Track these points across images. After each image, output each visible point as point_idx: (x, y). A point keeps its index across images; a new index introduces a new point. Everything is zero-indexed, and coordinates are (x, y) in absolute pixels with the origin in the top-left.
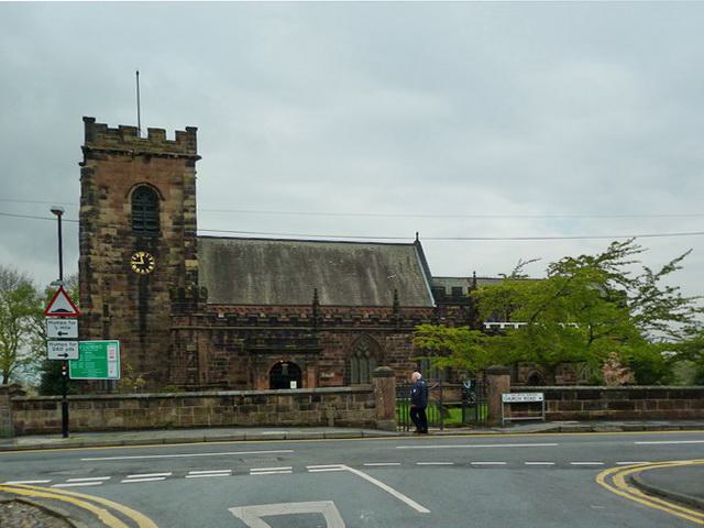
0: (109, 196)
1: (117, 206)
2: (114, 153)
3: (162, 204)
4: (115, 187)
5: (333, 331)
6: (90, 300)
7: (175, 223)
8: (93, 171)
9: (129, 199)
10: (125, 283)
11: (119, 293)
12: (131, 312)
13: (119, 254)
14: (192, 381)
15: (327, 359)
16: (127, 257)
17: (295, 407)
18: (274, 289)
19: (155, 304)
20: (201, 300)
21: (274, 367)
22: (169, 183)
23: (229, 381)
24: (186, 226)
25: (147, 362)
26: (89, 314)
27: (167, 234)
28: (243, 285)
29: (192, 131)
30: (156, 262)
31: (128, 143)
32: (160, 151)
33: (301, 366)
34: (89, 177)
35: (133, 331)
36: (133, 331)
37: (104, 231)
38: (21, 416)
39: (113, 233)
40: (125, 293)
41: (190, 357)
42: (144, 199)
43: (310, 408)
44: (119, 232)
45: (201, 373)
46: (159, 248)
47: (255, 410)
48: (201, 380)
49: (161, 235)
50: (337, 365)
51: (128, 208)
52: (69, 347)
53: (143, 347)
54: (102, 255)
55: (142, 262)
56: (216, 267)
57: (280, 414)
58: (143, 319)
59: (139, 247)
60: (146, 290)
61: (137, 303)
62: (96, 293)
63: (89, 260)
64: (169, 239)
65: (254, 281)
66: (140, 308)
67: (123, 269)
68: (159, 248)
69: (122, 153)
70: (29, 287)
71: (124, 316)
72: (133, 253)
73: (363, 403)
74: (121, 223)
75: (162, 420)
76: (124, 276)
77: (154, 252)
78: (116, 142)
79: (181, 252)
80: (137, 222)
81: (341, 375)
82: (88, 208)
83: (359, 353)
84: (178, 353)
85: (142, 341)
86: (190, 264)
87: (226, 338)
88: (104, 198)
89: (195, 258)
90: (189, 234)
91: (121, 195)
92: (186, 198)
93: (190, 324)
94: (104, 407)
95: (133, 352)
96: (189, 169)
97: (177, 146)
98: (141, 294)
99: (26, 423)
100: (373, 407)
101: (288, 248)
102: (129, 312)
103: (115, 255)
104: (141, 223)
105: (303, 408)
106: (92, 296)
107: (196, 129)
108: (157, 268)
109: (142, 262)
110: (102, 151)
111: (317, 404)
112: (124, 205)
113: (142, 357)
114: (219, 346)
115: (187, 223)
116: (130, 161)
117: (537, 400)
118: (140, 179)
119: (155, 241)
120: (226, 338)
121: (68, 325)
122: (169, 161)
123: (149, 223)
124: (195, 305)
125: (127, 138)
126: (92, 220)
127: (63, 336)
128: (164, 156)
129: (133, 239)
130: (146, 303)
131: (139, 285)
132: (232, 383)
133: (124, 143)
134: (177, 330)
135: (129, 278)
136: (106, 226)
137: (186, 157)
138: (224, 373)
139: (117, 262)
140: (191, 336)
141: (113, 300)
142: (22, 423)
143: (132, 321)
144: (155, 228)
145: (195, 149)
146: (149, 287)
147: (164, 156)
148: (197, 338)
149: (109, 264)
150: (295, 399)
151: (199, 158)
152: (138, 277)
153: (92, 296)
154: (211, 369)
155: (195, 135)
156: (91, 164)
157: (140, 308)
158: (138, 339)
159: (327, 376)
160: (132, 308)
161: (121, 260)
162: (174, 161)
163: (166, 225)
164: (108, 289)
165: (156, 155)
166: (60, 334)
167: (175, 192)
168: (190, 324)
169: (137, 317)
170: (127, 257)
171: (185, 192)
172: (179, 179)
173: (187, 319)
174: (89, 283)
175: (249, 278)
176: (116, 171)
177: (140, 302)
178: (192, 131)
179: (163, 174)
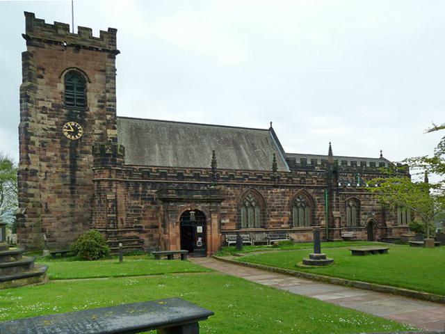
3: (89, 85)
11: (53, 154)
12: (63, 169)
14: (111, 226)
22: (95, 70)
24: (108, 103)
29: (113, 32)
32: (87, 44)
37: (41, 104)
39: (49, 106)
41: (110, 205)
48: (120, 225)
50: (230, 213)
53: (73, 197)
59: (70, 118)
60: (76, 152)
61: (68, 163)
69: (56, 43)
74: (55, 98)
77: (82, 122)
83: (247, 204)
84: (100, 202)
85: (72, 193)
90: (110, 110)
92: (107, 82)
93: (110, 176)
95: (64, 201)
96: (110, 60)
97: (101, 42)
98: (71, 156)
107: (116, 30)
108: (85, 136)
110: (39, 40)
115: (109, 101)
119: (83, 114)
122: (94, 52)
128: (91, 49)
129: (65, 111)
134: (99, 181)
137: (108, 51)
140: (110, 186)
141: (48, 159)
145: (115, 46)
146: (78, 150)
148: (116, 188)
151: (118, 52)
155: (115, 35)
160: (64, 166)
162: (99, 53)
165: (84, 47)
167: (98, 76)
168: (110, 176)
171: (107, 77)
172: (102, 67)
173: (107, 172)
178: (113, 32)
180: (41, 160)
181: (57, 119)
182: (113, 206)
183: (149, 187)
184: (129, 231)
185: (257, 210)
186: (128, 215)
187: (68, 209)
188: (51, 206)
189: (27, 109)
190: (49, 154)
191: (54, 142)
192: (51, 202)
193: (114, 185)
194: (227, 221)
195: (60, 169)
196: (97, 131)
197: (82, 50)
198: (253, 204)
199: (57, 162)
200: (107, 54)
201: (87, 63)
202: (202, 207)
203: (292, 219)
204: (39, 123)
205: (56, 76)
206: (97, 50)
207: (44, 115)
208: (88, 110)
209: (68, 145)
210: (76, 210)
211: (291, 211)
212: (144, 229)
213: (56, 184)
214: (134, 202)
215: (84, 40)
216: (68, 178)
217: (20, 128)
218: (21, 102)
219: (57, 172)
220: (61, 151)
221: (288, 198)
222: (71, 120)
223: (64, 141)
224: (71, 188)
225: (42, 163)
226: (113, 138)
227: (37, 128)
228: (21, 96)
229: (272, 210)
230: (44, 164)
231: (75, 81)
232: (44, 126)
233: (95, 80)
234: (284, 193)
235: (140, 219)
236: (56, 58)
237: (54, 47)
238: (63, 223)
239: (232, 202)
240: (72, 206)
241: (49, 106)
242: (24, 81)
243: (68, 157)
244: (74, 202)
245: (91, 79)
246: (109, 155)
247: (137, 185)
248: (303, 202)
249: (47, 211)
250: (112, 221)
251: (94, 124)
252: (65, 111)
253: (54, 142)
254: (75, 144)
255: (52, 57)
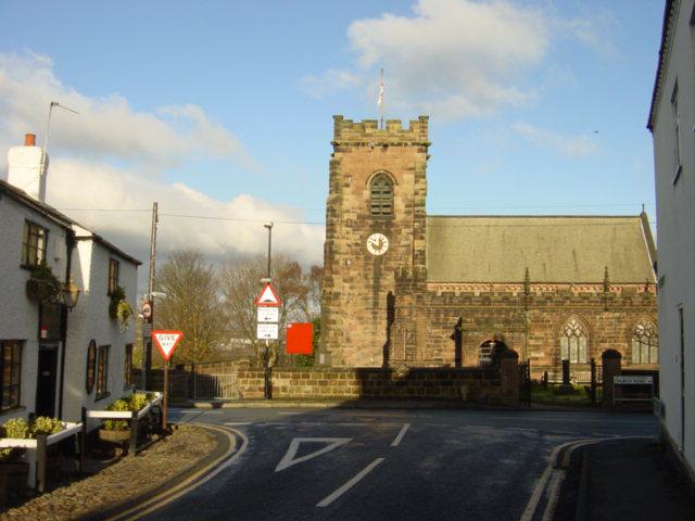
1: (358, 192)
2: (358, 144)
3: (396, 188)
5: (544, 310)
11: (356, 273)
12: (366, 291)
15: (537, 338)
37: (346, 217)
39: (354, 218)
46: (392, 229)
48: (418, 357)
50: (546, 344)
51: (367, 194)
53: (375, 323)
59: (375, 229)
60: (380, 269)
61: (371, 282)
68: (392, 229)
69: (363, 144)
74: (360, 209)
77: (387, 234)
81: (551, 355)
83: (569, 332)
85: (375, 318)
87: (442, 316)
88: (347, 185)
95: (366, 328)
98: (375, 274)
103: (355, 237)
110: (347, 144)
117: (647, 382)
118: (378, 167)
119: (389, 224)
120: (442, 316)
124: (414, 285)
128: (399, 144)
129: (370, 222)
131: (374, 264)
136: (348, 211)
139: (357, 244)
141: (351, 280)
146: (382, 266)
159: (537, 355)
160: (367, 287)
161: (359, 242)
165: (393, 144)
167: (409, 177)
170: (364, 239)
171: (416, 177)
180: (345, 281)
181: (361, 233)
182: (412, 336)
183: (451, 314)
185: (584, 341)
186: (428, 346)
187: (369, 338)
188: (352, 334)
189: (332, 225)
190: (353, 273)
191: (358, 258)
192: (352, 330)
193: (415, 313)
194: (542, 355)
195: (364, 291)
196: (403, 243)
197: (389, 148)
198: (578, 332)
199: (359, 282)
200: (416, 147)
201: (393, 161)
203: (631, 353)
204: (344, 237)
205: (362, 182)
206: (406, 145)
207: (348, 229)
208: (394, 218)
209: (372, 261)
210: (378, 338)
211: (629, 342)
213: (359, 308)
214: (434, 331)
215: (392, 136)
216: (371, 301)
217: (325, 245)
218: (327, 216)
219: (360, 294)
220: (364, 270)
221: (623, 326)
222: (375, 231)
223: (368, 256)
224: (375, 313)
225: (345, 284)
226: (420, 251)
227: (342, 244)
228: (328, 210)
229: (602, 341)
230: (347, 285)
231: (381, 185)
232: (349, 242)
234: (618, 318)
235: (440, 350)
236: (363, 161)
237: (361, 148)
238: (363, 354)
239: (549, 331)
240: (373, 333)
241: (354, 218)
242: (330, 193)
243: (371, 276)
244: (376, 329)
247: (437, 313)
248: (648, 330)
249: (348, 340)
250: (409, 357)
251: (400, 233)
252: (370, 222)
253: (358, 258)
254: (380, 259)
255: (359, 161)
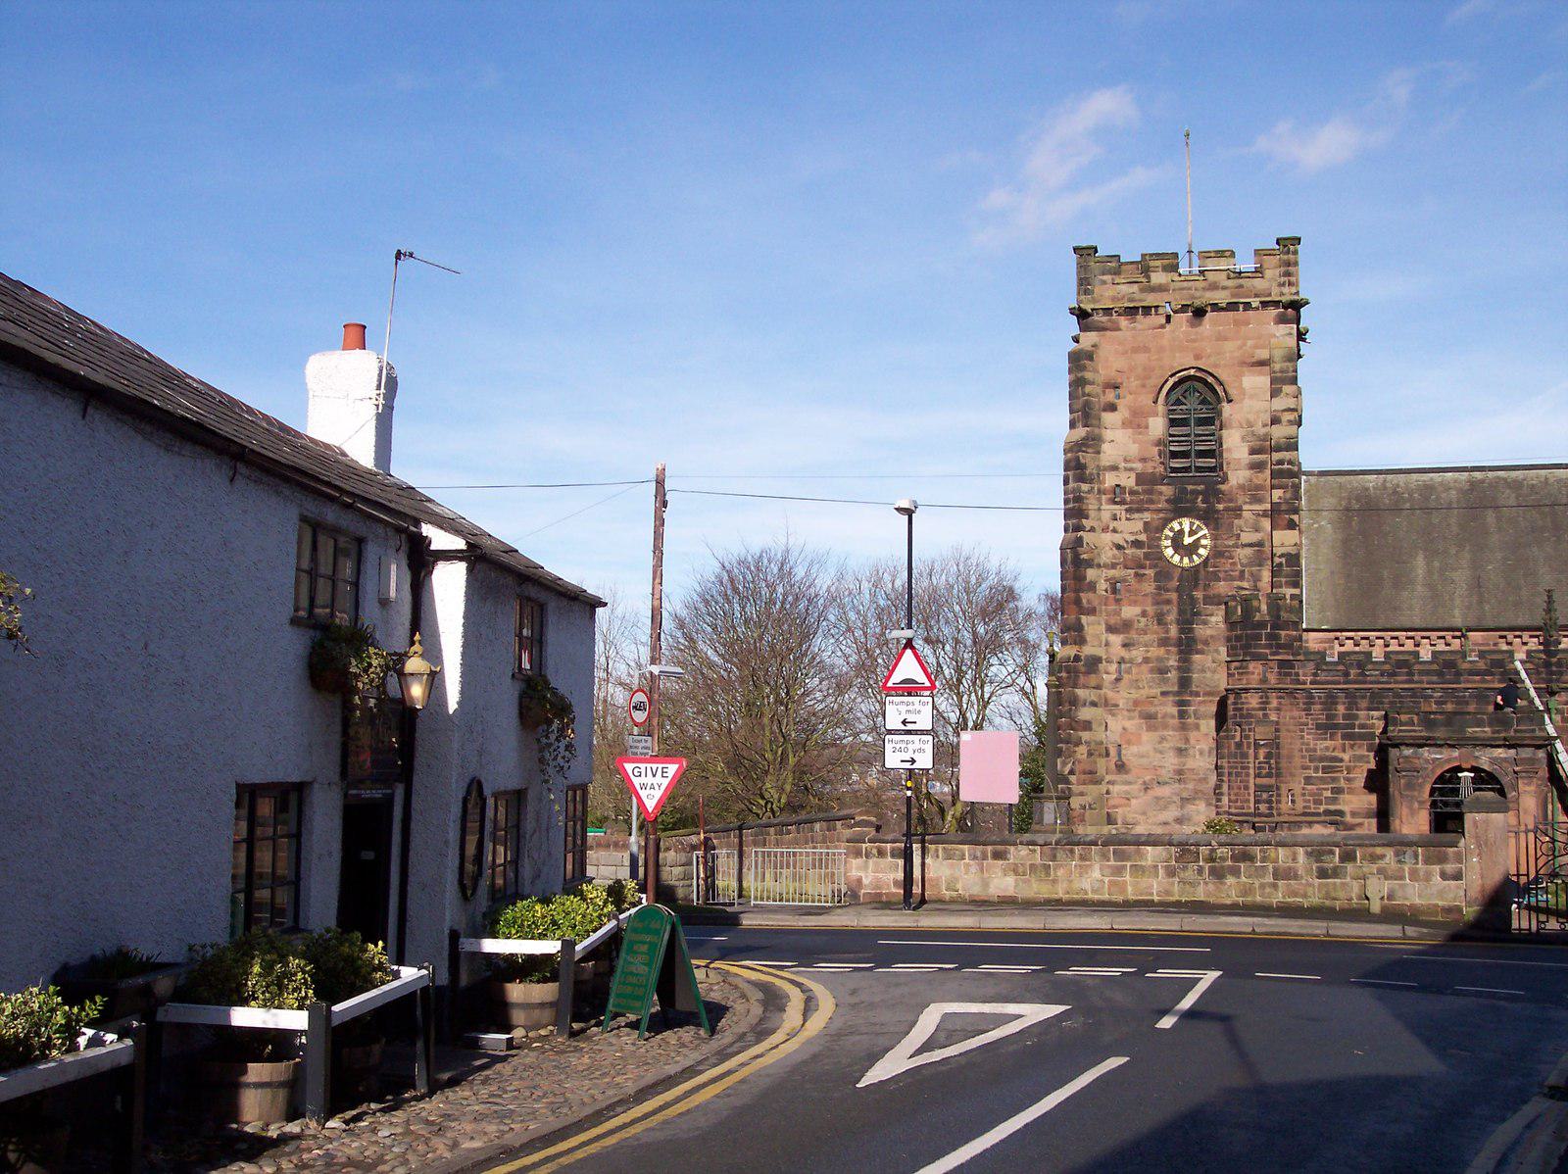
0: (1121, 404)
1: (1136, 422)
2: (1131, 312)
4: (1134, 383)
6: (1079, 628)
7: (1253, 452)
8: (1090, 356)
9: (1161, 408)
10: (1149, 587)
11: (1137, 610)
12: (1162, 651)
13: (1140, 526)
16: (1154, 530)
17: (1309, 871)
18: (1477, 584)
19: (1209, 632)
20: (1286, 625)
21: (1441, 779)
22: (1243, 363)
23: (1346, 808)
25: (1191, 764)
26: (1077, 658)
27: (1237, 476)
28: (1400, 582)
30: (1214, 538)
31: (1161, 289)
32: (1222, 298)
33: (1505, 780)
34: (1084, 368)
35: (1163, 694)
36: (1163, 694)
37: (1110, 480)
38: (859, 868)
39: (1128, 481)
40: (1150, 609)
42: (1192, 403)
43: (1336, 873)
44: (1141, 479)
45: (1284, 791)
47: (1236, 872)
49: (1225, 480)
51: (1157, 426)
52: (917, 746)
53: (1184, 727)
54: (1105, 530)
55: (1187, 540)
56: (1345, 542)
57: (1280, 883)
58: (1185, 666)
59: (1179, 508)
60: (1193, 601)
61: (1174, 631)
62: (1092, 611)
63: (1079, 541)
64: (1241, 487)
65: (1429, 572)
66: (1179, 643)
67: (1147, 556)
68: (1220, 507)
69: (1147, 310)
70: (1011, 590)
71: (1146, 660)
72: (1167, 521)
73: (1437, 868)
75: (1076, 885)
76: (1150, 572)
77: (1209, 517)
78: (1135, 287)
79: (1265, 514)
80: (1174, 455)
82: (1081, 432)
85: (1182, 715)
86: (1284, 540)
87: (1341, 709)
88: (1112, 408)
89: (1292, 525)
91: (1146, 399)
94: (985, 857)
95: (1163, 739)
98: (1181, 612)
99: (865, 881)
100: (1458, 876)
101: (1516, 485)
102: (1156, 652)
103: (1131, 528)
104: (1185, 455)
105: (1323, 874)
106: (1084, 619)
108: (1217, 553)
109: (1187, 540)
110: (1107, 311)
111: (1349, 866)
112: (1151, 420)
113: (1180, 752)
114: (1327, 728)
115: (1278, 449)
116: (1162, 327)
118: (1184, 361)
119: (1212, 493)
120: (1341, 709)
121: (917, 707)
122: (1240, 314)
123: (1202, 454)
124: (1272, 637)
125: (1158, 278)
126: (1086, 458)
127: (910, 727)
128: (1232, 307)
129: (1167, 491)
130: (1191, 630)
132: (1354, 814)
133: (1153, 289)
135: (1158, 577)
136: (1114, 468)
137: (1276, 304)
138: (1338, 791)
139: (1137, 544)
140: (1264, 704)
142: (859, 881)
143: (1162, 671)
144: (1211, 462)
146: (1199, 594)
147: (1232, 307)
149: (1119, 547)
150: (1309, 854)
152: (1177, 574)
153: (1084, 619)
154: (1308, 780)
156: (1089, 339)
157: (1179, 643)
158: (1174, 710)
160: (1164, 642)
161: (1143, 537)
163: (1236, 455)
164: (1118, 601)
165: (1215, 307)
166: (904, 722)
169: (1173, 662)
170: (1154, 530)
172: (1264, 354)
174: (1077, 591)
175: (1420, 563)
176: (1136, 350)
177: (1181, 631)
179: (1229, 346)
184: (1310, 824)
193: (1274, 703)
202: (1493, 761)
206: (1247, 306)
212: (1348, 819)
233: (1243, 392)
245: (1232, 392)
246: (1262, 625)
